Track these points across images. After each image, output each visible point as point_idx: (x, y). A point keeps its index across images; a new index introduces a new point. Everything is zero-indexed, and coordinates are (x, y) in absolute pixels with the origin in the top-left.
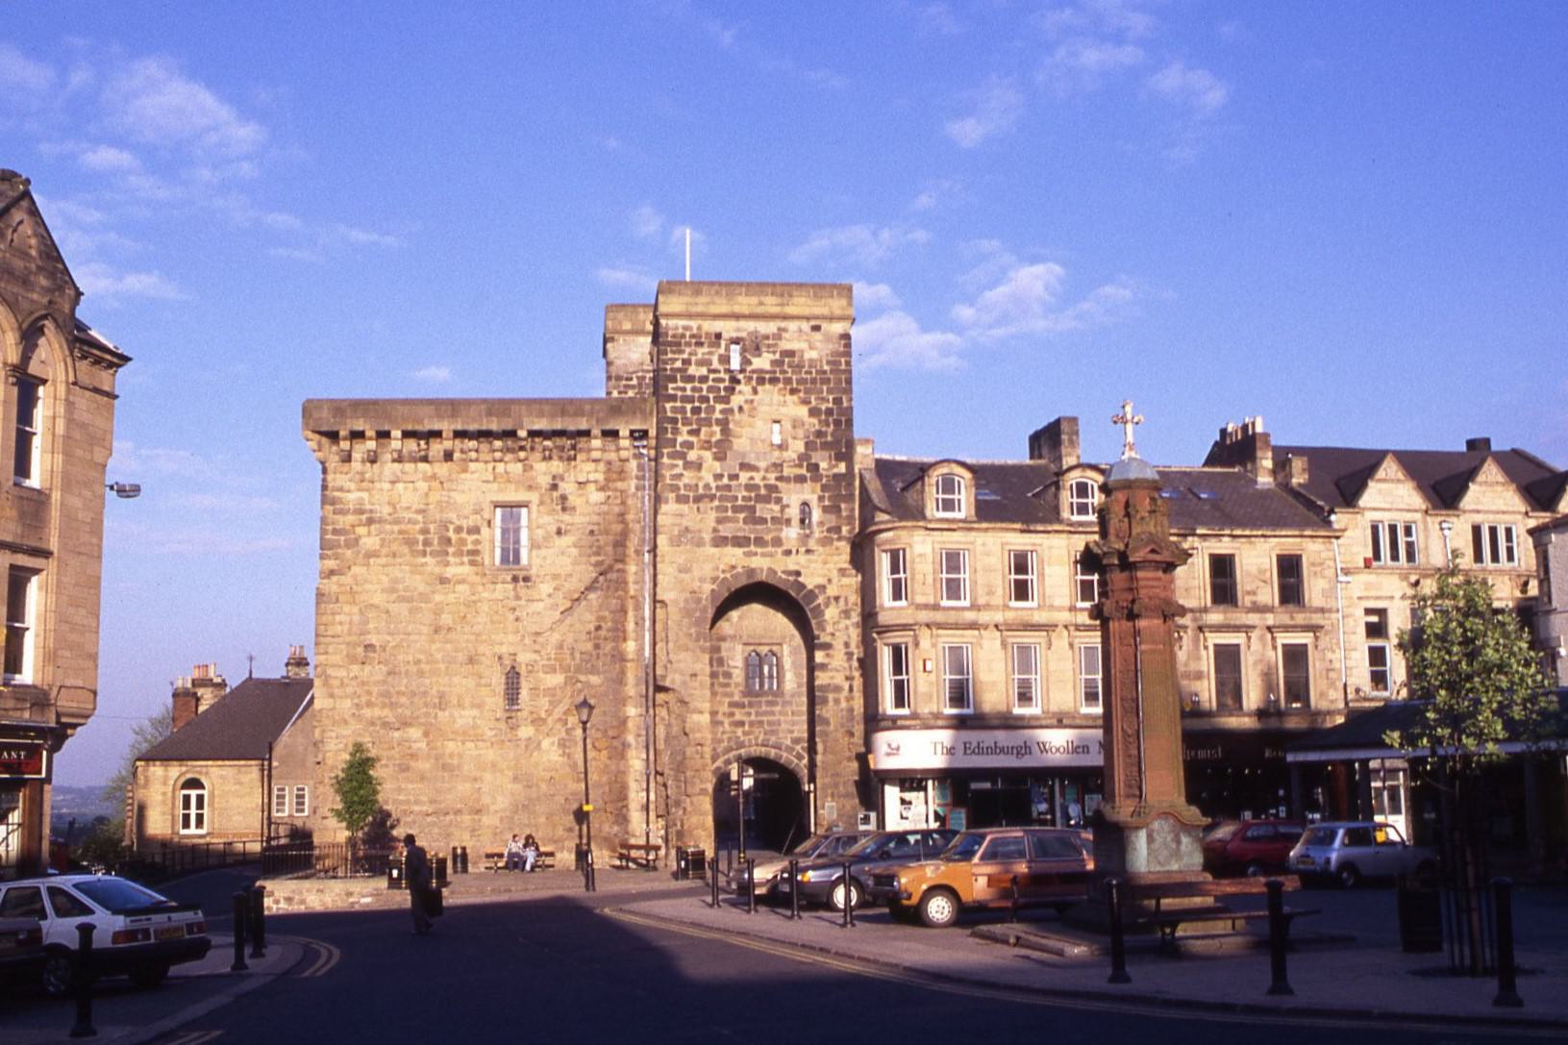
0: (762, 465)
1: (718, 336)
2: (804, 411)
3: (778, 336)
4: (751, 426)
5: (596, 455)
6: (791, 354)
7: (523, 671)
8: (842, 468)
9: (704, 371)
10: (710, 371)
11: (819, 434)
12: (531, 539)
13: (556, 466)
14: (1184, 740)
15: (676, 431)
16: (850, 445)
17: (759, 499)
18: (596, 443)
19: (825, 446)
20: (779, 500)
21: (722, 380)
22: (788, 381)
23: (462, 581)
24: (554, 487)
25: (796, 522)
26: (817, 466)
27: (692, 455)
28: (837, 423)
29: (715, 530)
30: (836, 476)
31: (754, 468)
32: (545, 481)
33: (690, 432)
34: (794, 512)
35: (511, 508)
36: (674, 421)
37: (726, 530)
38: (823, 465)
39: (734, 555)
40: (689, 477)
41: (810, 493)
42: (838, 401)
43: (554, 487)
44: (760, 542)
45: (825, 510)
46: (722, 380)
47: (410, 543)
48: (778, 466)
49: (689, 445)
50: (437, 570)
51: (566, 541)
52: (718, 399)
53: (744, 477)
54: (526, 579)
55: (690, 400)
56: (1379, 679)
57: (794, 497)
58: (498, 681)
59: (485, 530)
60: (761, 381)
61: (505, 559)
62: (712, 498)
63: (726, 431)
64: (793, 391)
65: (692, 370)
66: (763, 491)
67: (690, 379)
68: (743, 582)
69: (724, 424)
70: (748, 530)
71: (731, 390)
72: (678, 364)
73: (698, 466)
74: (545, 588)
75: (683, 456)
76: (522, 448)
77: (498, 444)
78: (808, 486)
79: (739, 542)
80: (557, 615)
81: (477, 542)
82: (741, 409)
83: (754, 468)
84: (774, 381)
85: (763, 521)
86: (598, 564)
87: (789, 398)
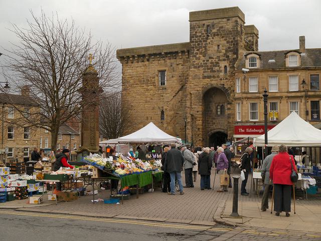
0: (214, 57)
1: (204, 25)
2: (225, 42)
3: (219, 23)
4: (212, 47)
5: (181, 57)
6: (222, 27)
7: (164, 110)
8: (235, 56)
9: (200, 34)
10: (202, 34)
11: (229, 48)
12: (167, 79)
13: (172, 61)
14: (219, 133)
15: (194, 50)
16: (237, 50)
17: (214, 66)
18: (180, 54)
19: (231, 51)
20: (219, 66)
21: (205, 36)
22: (221, 35)
23: (152, 90)
24: (171, 66)
25: (223, 71)
26: (228, 56)
27: (198, 56)
28: (234, 44)
29: (203, 75)
30: (233, 59)
31: (212, 58)
32: (169, 64)
33: (197, 50)
34: (223, 69)
35: (162, 72)
36: (193, 48)
37: (206, 74)
38: (230, 56)
39: (207, 81)
40: (197, 62)
41: (226, 63)
42: (234, 39)
43: (171, 66)
44: (214, 77)
45: (230, 68)
46: (205, 36)
47: (140, 81)
48: (219, 57)
49: (197, 54)
50: (146, 87)
51: (174, 78)
52: (204, 41)
53: (210, 60)
54: (165, 89)
55: (196, 42)
56: (254, 115)
57: (222, 64)
58: (160, 113)
59: (156, 77)
60: (214, 35)
61: (161, 84)
62: (202, 66)
63: (206, 49)
64: (223, 37)
65: (198, 34)
66: (215, 64)
67: (197, 37)
68: (210, 87)
69: (205, 47)
70: (211, 74)
71: (207, 39)
72: (194, 33)
73: (199, 59)
74: (169, 91)
75: (195, 56)
76: (163, 57)
77: (158, 56)
78: (226, 62)
79: (209, 77)
80: (172, 97)
81: (154, 80)
82: (209, 43)
83: (212, 58)
84: (218, 35)
85: (215, 71)
86: (182, 84)
87: (221, 39)
